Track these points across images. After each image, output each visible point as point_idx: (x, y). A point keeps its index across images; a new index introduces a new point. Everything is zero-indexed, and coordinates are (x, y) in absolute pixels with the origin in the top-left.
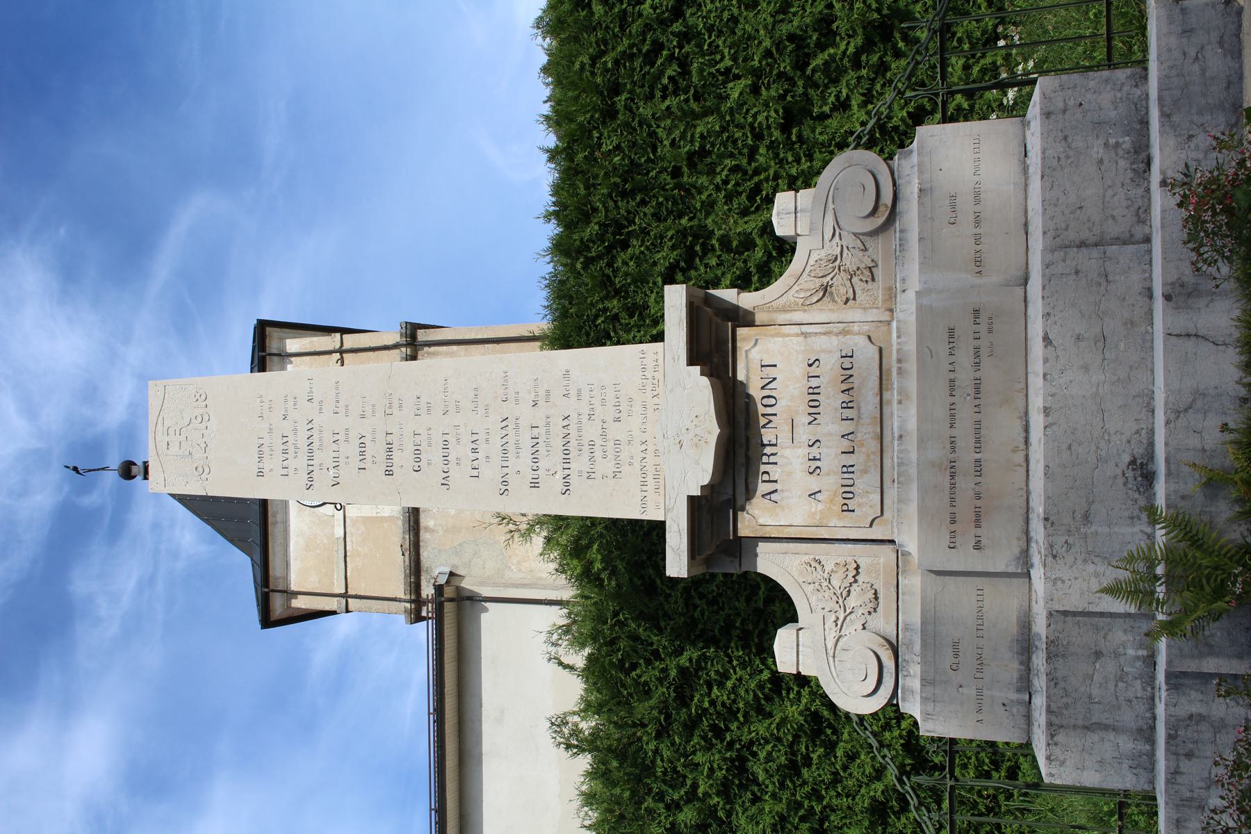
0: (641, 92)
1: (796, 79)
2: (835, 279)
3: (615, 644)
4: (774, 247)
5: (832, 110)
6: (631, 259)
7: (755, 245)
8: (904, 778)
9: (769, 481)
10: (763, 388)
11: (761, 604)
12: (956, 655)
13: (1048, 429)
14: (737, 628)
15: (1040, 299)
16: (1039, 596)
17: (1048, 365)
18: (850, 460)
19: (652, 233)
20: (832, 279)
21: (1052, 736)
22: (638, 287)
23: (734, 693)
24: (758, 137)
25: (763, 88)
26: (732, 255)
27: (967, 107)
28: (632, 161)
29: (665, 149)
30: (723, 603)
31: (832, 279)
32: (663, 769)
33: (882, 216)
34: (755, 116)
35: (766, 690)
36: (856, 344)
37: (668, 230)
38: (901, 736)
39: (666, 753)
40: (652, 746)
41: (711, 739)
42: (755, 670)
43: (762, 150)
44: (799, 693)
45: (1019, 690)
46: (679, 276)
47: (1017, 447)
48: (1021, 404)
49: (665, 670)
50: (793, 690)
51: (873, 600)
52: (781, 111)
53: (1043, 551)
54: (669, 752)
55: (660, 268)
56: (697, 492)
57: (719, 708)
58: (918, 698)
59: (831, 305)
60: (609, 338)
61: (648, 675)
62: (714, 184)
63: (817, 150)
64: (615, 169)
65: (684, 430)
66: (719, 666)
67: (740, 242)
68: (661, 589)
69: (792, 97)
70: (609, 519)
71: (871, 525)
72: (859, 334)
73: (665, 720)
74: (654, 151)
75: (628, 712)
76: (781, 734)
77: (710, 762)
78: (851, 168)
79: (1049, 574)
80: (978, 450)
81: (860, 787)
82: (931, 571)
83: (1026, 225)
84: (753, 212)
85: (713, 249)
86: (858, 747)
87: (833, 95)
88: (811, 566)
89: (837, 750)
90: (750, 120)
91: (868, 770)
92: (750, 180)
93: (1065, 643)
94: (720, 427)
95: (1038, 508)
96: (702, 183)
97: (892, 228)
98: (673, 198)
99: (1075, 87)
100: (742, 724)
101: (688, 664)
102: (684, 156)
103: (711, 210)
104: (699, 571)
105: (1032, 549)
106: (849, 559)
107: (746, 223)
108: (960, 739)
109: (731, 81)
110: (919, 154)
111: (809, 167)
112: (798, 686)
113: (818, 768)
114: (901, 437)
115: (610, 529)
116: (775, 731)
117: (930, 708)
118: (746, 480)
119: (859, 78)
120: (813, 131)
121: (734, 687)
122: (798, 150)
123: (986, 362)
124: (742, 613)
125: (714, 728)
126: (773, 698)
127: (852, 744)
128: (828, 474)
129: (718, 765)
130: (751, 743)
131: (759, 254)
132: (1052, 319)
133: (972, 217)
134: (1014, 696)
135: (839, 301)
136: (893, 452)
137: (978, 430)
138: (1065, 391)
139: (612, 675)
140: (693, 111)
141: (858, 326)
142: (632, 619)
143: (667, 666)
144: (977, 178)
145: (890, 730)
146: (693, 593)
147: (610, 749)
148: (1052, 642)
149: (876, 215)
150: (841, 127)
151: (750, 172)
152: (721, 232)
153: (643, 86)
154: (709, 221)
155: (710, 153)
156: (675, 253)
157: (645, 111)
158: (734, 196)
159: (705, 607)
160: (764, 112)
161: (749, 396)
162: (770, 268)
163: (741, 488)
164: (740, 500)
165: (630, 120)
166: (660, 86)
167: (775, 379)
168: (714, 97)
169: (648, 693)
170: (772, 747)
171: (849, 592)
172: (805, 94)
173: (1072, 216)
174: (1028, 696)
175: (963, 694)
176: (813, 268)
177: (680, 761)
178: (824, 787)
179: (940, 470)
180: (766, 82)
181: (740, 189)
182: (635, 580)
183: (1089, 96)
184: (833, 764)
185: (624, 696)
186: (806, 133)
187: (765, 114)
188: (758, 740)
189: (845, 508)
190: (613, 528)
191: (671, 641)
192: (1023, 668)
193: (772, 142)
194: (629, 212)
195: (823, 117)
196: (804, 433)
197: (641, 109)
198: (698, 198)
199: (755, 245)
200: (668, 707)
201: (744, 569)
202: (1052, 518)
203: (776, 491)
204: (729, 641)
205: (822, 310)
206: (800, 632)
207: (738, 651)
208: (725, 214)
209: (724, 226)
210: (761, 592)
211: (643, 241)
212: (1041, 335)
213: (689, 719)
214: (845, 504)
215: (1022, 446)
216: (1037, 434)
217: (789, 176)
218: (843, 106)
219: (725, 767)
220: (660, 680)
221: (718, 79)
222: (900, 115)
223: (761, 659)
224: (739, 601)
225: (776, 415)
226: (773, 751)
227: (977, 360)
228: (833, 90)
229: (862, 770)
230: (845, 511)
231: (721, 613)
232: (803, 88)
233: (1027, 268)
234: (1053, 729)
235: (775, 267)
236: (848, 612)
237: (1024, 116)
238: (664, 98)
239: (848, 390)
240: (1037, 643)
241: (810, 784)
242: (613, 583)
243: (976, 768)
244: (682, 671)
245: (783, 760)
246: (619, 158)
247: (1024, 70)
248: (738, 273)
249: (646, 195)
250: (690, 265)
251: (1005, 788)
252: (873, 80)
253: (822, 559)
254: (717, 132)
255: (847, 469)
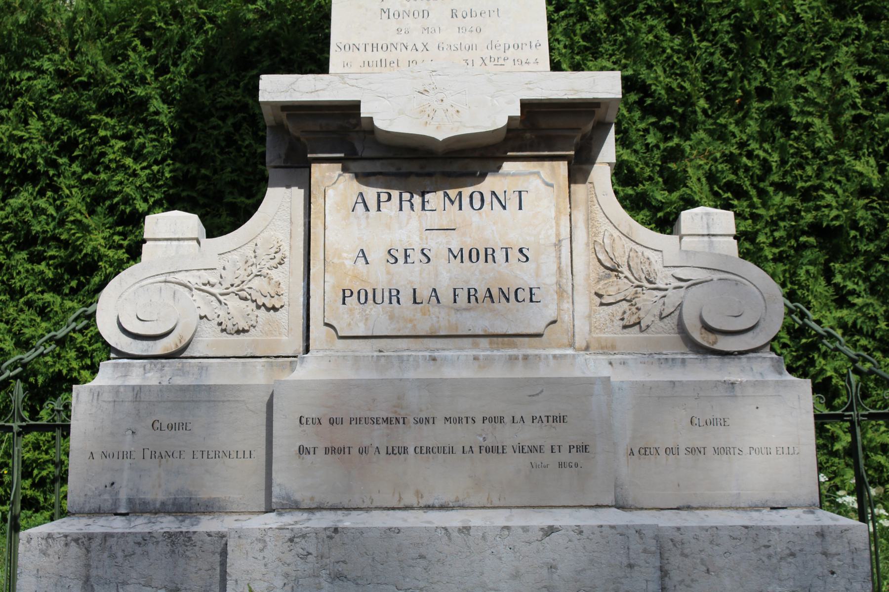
0: (867, 48)
1: (877, 242)
2: (626, 281)
3: (175, 18)
4: (669, 214)
5: (836, 285)
6: (656, 37)
7: (670, 191)
8: (19, 369)
9: (379, 202)
10: (493, 193)
11: (229, 199)
12: (171, 427)
13: (443, 532)
14: (198, 171)
15: (600, 524)
16: (244, 523)
17: (520, 531)
18: (406, 297)
19: (688, 63)
20: (626, 277)
21: (76, 540)
22: (621, 45)
23: (117, 168)
24: (806, 195)
25: (867, 201)
26: (659, 163)
27: (835, 448)
28: (780, 37)
29: (794, 80)
30: (229, 153)
31: (626, 277)
32: (18, 79)
33: (703, 338)
34: (831, 191)
35: (122, 207)
36: (546, 306)
37: (692, 83)
38: (71, 370)
39: (38, 84)
40: (47, 65)
41: (58, 139)
42: (147, 192)
43: (789, 200)
44: (120, 246)
45: (130, 501)
46: (633, 97)
47: (422, 497)
48: (474, 501)
49: (143, 81)
50: (124, 240)
51: (235, 328)
52: (837, 223)
53: (298, 526)
54: (40, 86)
55: (644, 72)
56: (364, 112)
57: (98, 149)
58: (118, 382)
59: (593, 276)
60: (558, 9)
61: (137, 61)
62: (748, 140)
63: (787, 267)
64: (771, 16)
65: (440, 96)
66: (150, 149)
67: (676, 172)
68: (244, 76)
69: (855, 237)
70: (330, 9)
71: (327, 325)
72: (559, 309)
73: (81, 82)
74: (791, 66)
75: (89, 35)
76: (69, 225)
77: (29, 138)
78: (762, 302)
79: (270, 533)
80: (418, 450)
81: (7, 323)
82: (272, 396)
83: (689, 508)
84: (711, 189)
85: (666, 139)
86: (57, 319)
87: (855, 287)
88: (276, 253)
89: (51, 294)
90: (828, 185)
91: (28, 332)
92: (752, 184)
93: (188, 553)
94: (444, 140)
95: (349, 521)
96: (749, 125)
97: (687, 350)
98: (731, 90)
99: (854, 566)
100: (79, 178)
101: (152, 109)
102: (784, 103)
103: (716, 137)
104: (269, 118)
105: (300, 514)
106: (285, 299)
107: (699, 179)
108: (69, 441)
109: (877, 162)
110: (777, 382)
111: (766, 257)
112: (129, 246)
113: (27, 271)
114: (434, 359)
115: (319, 12)
116: (72, 218)
117: (106, 396)
118: (380, 173)
119: (875, 319)
120: (811, 263)
121: (125, 168)
122: (788, 244)
123: (524, 460)
124: (216, 176)
125: (73, 143)
126: (113, 215)
127: (59, 311)
128: (388, 273)
129: (27, 148)
130: (56, 189)
131: (660, 195)
132: (575, 537)
133: (699, 444)
134: (123, 496)
135: (600, 286)
136: (416, 350)
137: (442, 450)
138: (490, 551)
139: (135, 15)
140: (840, 114)
141: (568, 308)
142: (207, 40)
143: (149, 84)
144: (746, 450)
145: (78, 357)
146: (240, 115)
147: (40, 12)
148: (190, 538)
149: (703, 330)
150: (815, 297)
151: (762, 185)
152: (688, 149)
153: (875, 51)
154: (701, 134)
155: (787, 135)
156: (663, 92)
157: (844, 54)
158: (733, 165)
159: (223, 131)
160: (837, 202)
161: (483, 176)
162: (641, 209)
163: (369, 167)
164: (354, 166)
165: (833, 35)
166: (874, 72)
167: (504, 208)
168: (857, 141)
169: (113, 60)
170: (52, 215)
171: (246, 299)
172: (857, 253)
173: (698, 561)
174: (123, 511)
175: (125, 435)
176: (640, 254)
177: (30, 100)
178: (5, 278)
179: (395, 406)
180: (875, 205)
181: (741, 173)
182: (255, 43)
183: (843, 582)
184: (34, 290)
185: (108, 30)
186: (808, 254)
187: (834, 204)
188: (60, 197)
189: (348, 293)
190: (320, 15)
191: (180, 89)
192: (158, 505)
193: (799, 211)
194: (715, 33)
195: (828, 274)
196: (438, 244)
197: (845, 49)
198: (731, 120)
199: (670, 191)
200: (97, 86)
201: (271, 173)
202: (337, 537)
203: (367, 210)
204: (183, 161)
205: (588, 265)
206: (195, 242)
207: (170, 172)
208: (710, 154)
209: (695, 152)
210: (243, 199)
211: (678, 52)
212: (556, 524)
213: (82, 112)
214: (352, 293)
215: (423, 503)
216: (437, 518)
217: (756, 233)
218: (842, 299)
219: (25, 156)
220: (131, 76)
221: (879, 145)
222: (827, 368)
223: (161, 200)
224: (232, 172)
225: (460, 209)
226: (48, 216)
227: (526, 449)
228: (862, 287)
229: (28, 324)
230: (344, 293)
231: (217, 151)
232: (865, 251)
233: (637, 509)
234: (85, 541)
235: (645, 213)
236: (221, 298)
237: (821, 507)
238: (859, 78)
239: (491, 296)
240: (187, 521)
241: (8, 261)
242: (250, 16)
243: (36, 461)
244: (143, 103)
245: (35, 228)
246: (784, 20)
247: (880, 516)
248: (637, 170)
249: (736, 55)
250: (647, 111)
251: (10, 495)
252: (871, 336)
253: (285, 266)
254: (814, 144)
255: (395, 296)
